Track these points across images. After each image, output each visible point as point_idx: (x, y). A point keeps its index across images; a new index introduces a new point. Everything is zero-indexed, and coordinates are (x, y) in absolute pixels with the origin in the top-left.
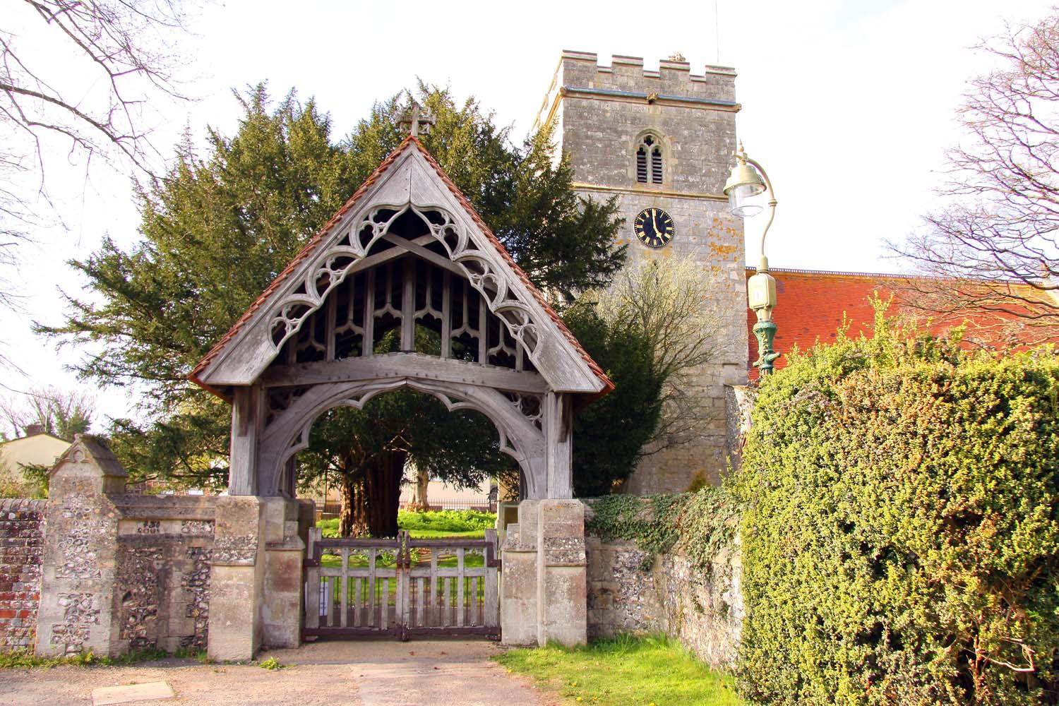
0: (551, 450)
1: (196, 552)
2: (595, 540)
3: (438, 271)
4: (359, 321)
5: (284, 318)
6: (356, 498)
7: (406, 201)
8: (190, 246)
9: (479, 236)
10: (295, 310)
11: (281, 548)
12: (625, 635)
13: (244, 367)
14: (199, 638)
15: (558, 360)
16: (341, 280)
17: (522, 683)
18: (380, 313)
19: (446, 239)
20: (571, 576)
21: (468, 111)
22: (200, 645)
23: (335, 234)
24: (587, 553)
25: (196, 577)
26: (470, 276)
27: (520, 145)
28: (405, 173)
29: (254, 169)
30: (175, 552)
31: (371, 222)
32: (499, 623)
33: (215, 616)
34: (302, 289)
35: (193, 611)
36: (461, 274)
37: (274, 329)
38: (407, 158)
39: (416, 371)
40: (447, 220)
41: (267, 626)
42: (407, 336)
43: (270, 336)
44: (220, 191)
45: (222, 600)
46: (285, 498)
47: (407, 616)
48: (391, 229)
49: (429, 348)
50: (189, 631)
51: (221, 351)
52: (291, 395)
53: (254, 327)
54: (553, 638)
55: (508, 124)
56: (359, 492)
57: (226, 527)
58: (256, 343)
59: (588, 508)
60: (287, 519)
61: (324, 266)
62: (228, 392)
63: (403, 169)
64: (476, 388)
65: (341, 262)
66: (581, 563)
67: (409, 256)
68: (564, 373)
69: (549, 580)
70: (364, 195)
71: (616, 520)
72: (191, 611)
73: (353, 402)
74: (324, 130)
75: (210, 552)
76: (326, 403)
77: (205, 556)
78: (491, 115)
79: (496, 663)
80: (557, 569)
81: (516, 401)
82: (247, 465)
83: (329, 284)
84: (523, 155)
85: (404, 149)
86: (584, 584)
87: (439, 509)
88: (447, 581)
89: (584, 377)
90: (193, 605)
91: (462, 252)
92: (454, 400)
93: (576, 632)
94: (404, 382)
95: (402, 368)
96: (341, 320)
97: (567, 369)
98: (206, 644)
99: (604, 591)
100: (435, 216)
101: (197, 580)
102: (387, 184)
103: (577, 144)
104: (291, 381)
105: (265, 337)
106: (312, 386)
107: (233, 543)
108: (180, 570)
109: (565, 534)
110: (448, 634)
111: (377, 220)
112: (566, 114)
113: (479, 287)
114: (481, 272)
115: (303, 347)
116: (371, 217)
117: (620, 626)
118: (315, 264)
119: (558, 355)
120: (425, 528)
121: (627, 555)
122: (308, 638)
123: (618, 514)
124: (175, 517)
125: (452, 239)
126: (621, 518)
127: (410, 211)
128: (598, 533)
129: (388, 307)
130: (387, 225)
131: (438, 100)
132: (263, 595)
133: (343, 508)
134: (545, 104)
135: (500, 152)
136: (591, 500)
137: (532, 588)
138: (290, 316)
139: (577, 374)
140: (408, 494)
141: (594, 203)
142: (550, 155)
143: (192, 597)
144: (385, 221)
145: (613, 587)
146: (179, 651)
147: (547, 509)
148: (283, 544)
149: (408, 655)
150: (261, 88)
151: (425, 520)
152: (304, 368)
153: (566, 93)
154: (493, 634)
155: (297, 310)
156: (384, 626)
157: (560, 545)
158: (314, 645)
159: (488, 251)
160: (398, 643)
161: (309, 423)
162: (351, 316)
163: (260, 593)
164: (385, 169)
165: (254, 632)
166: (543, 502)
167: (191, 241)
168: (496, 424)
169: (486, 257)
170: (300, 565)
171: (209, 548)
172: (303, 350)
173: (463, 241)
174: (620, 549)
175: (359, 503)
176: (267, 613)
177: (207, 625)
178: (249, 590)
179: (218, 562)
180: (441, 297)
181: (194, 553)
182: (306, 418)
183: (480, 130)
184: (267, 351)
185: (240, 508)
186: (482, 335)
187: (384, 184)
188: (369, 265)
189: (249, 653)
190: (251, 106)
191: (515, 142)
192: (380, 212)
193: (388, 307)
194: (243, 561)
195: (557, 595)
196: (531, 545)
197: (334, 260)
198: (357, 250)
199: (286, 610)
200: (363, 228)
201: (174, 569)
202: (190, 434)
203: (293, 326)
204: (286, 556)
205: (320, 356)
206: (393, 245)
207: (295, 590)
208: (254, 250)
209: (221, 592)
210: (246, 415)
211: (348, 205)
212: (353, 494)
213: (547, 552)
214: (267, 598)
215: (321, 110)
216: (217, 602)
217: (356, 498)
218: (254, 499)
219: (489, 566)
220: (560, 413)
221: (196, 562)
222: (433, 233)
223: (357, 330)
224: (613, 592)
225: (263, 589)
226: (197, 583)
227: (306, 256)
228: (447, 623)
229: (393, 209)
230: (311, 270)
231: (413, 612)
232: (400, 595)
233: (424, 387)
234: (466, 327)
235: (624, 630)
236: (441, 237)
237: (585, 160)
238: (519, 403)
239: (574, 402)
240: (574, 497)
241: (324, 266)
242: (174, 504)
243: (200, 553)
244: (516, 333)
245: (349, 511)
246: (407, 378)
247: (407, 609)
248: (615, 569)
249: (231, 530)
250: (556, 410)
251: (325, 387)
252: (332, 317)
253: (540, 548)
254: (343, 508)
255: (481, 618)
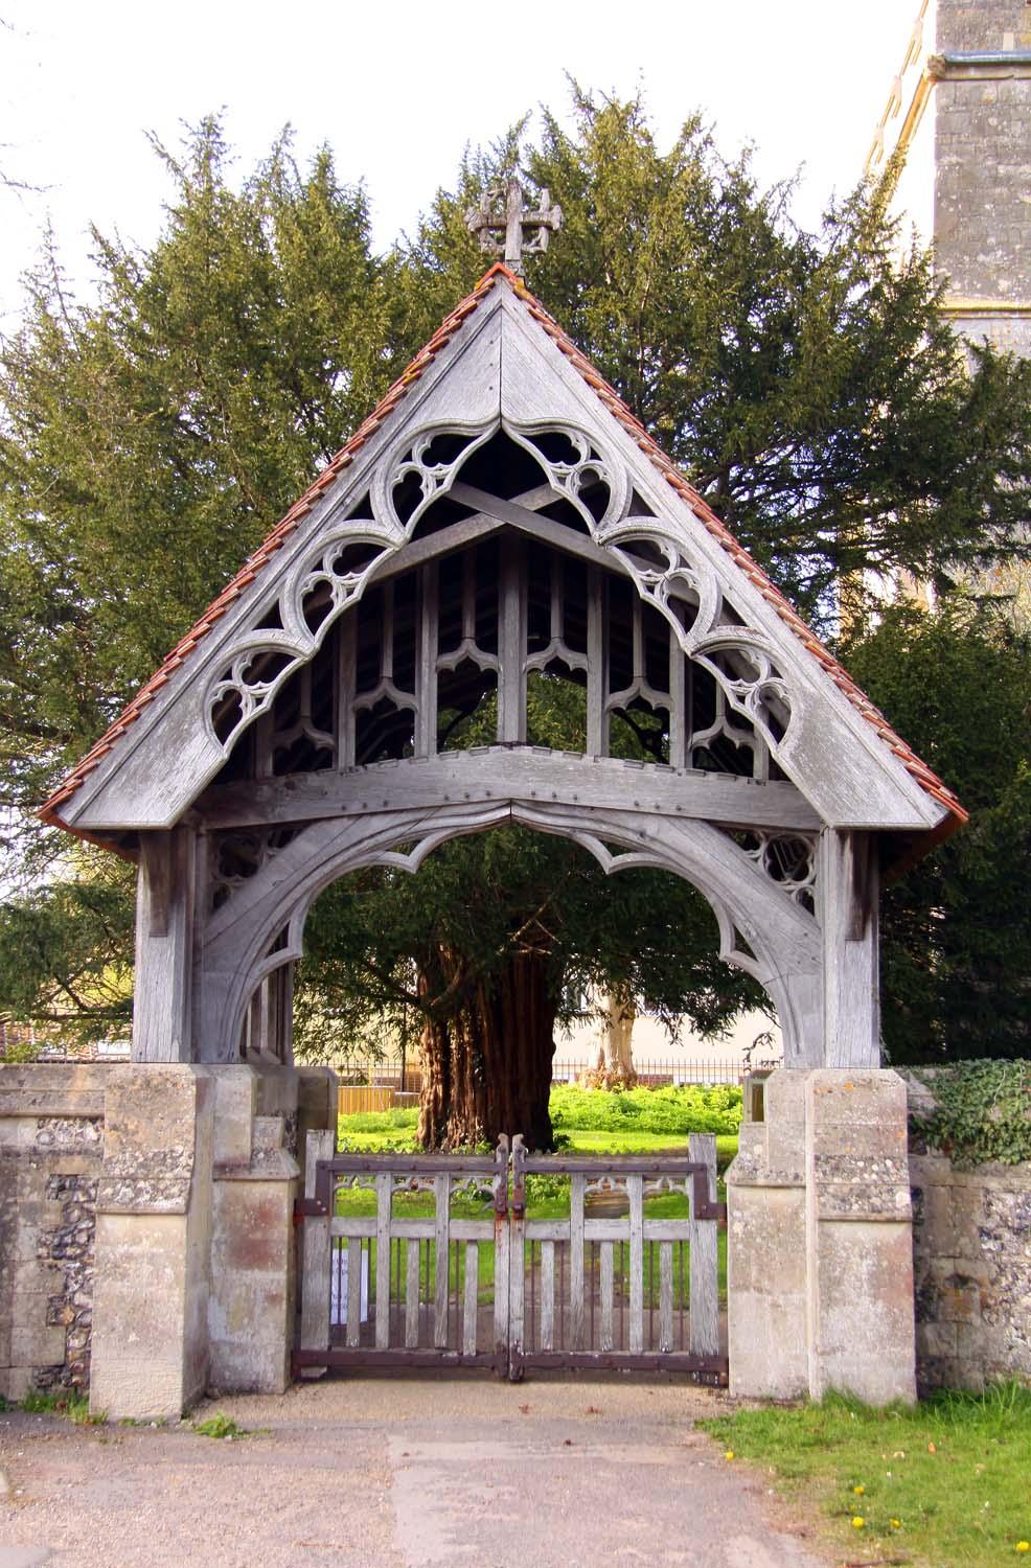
0: (832, 960)
1: (66, 1185)
2: (937, 1164)
3: (577, 566)
4: (406, 679)
5: (237, 682)
6: (455, 1057)
7: (492, 413)
8: (64, 505)
9: (655, 486)
10: (263, 662)
11: (245, 1175)
12: (1010, 1386)
13: (155, 790)
14: (74, 1371)
15: (838, 757)
16: (357, 595)
17: (748, 1482)
18: (451, 660)
19: (582, 495)
20: (878, 1245)
21: (688, 151)
22: (76, 1385)
23: (340, 494)
24: (916, 1193)
25: (68, 1239)
26: (638, 576)
27: (812, 224)
28: (484, 352)
29: (197, 324)
30: (24, 1184)
31: (417, 464)
32: (724, 1349)
33: (104, 1321)
34: (272, 620)
35: (62, 1313)
36: (619, 569)
37: (216, 707)
38: (490, 317)
39: (532, 786)
40: (584, 451)
41: (217, 1345)
42: (508, 709)
43: (209, 721)
44: (126, 379)
45: (120, 1287)
46: (260, 1067)
47: (518, 1327)
48: (461, 477)
49: (556, 727)
50: (54, 1355)
51: (107, 759)
52: (264, 845)
53: (173, 704)
54: (838, 1386)
55: (788, 174)
56: (460, 1046)
57: (126, 1132)
58: (180, 738)
59: (922, 1090)
60: (259, 1111)
61: (319, 567)
62: (125, 842)
63: (483, 341)
64: (665, 823)
65: (355, 555)
66: (899, 1215)
67: (506, 537)
68: (851, 787)
69: (826, 1252)
70: (401, 405)
71: (985, 1119)
72: (57, 1312)
73: (396, 858)
74: (354, 223)
75: (95, 1185)
76: (339, 860)
77: (87, 1193)
78: (746, 153)
79: (704, 1436)
80: (845, 1226)
81: (757, 847)
82: (169, 998)
83: (331, 605)
84: (824, 250)
85: (484, 295)
86: (906, 1263)
87: (658, 1082)
88: (607, 1251)
89: (896, 793)
90: (61, 1300)
91: (618, 521)
92: (615, 849)
93: (886, 1372)
94: (506, 812)
95: (502, 781)
96: (368, 678)
97: (859, 778)
98: (87, 1385)
99: (961, 1280)
100: (557, 444)
101: (68, 1246)
102: (449, 378)
103: (968, 200)
104: (263, 815)
105: (198, 724)
106: (306, 824)
107: (141, 1165)
108: (35, 1224)
109: (863, 1148)
110: (609, 1370)
111: (430, 459)
112: (943, 126)
113: (658, 601)
114: (663, 563)
115: (289, 739)
116: (417, 453)
117: (998, 1366)
118: (299, 563)
119: (835, 747)
120: (624, 1126)
121: (1010, 1199)
122: (305, 1373)
123: (988, 1104)
124: (22, 1111)
125: (597, 494)
126: (996, 1115)
127: (501, 436)
128: (945, 1148)
129: (469, 647)
130: (450, 470)
131: (616, 128)
132: (209, 1278)
133: (426, 1082)
134: (893, 103)
135: (769, 241)
136: (930, 1072)
137: (793, 1266)
138: (250, 677)
139: (881, 787)
140: (577, 1047)
141: (999, 353)
142: (886, 246)
143: (59, 1280)
144: (448, 461)
145: (981, 1272)
146: (32, 1397)
147: (823, 1092)
148: (250, 1167)
149: (515, 1414)
150: (210, 128)
151: (627, 1108)
152: (290, 786)
153: (945, 70)
154: (710, 1371)
155: (265, 664)
156: (470, 1347)
157: (852, 1173)
158: (318, 1387)
159: (678, 520)
160: (498, 1386)
161: (305, 900)
162: (388, 671)
163: (201, 1273)
164: (444, 345)
165: (187, 1356)
166: (816, 1074)
167: (68, 495)
168: (712, 900)
169: (671, 532)
170: (286, 1211)
171: (95, 1176)
172: (288, 742)
173: (619, 499)
174: (993, 1184)
175: (461, 1071)
176: (217, 1318)
177: (88, 1343)
178: (174, 1266)
179: (112, 1207)
180: (584, 616)
181: (62, 1188)
182: (295, 894)
183: (717, 193)
184: (203, 756)
185: (156, 1090)
186: (675, 700)
187: (443, 377)
188: (419, 558)
189: (175, 1403)
190: (191, 170)
191: (803, 218)
192: (436, 441)
193: (469, 647)
194: (163, 1204)
195: (846, 1287)
196: (791, 1171)
197: (339, 553)
198: (389, 528)
199: (258, 1310)
200: (400, 479)
201: (22, 1221)
202: (76, 926)
203: (258, 700)
204: (257, 1192)
205: (323, 760)
206: (467, 513)
207: (278, 1267)
208: (204, 511)
209: (117, 1270)
210: (167, 886)
211: (364, 430)
212: (446, 1051)
213: (822, 1187)
214: (218, 1286)
215: (345, 177)
216: (104, 1295)
217: (455, 1057)
218: (186, 1073)
219: (700, 1216)
220: (849, 876)
221: (66, 1207)
222: (553, 483)
223: (402, 699)
224: (980, 1285)
225: (208, 1265)
226: (69, 1251)
227: (280, 546)
228: (606, 1343)
229: (465, 432)
230: (291, 575)
231: (532, 1315)
232: (505, 1280)
233: (549, 820)
234: (639, 686)
235: (1008, 1373)
236: (570, 492)
237: (992, 240)
238: (761, 852)
239: (881, 852)
240: (885, 1064)
241: (319, 567)
242: (21, 1083)
243: (75, 1188)
244: (741, 699)
245: (440, 1088)
246: (511, 803)
247: (518, 1310)
248: (983, 1232)
249: (137, 1138)
250: (841, 870)
251: (335, 827)
252: (348, 674)
253: (809, 1177)
254: (426, 1082)
255: (681, 1339)
